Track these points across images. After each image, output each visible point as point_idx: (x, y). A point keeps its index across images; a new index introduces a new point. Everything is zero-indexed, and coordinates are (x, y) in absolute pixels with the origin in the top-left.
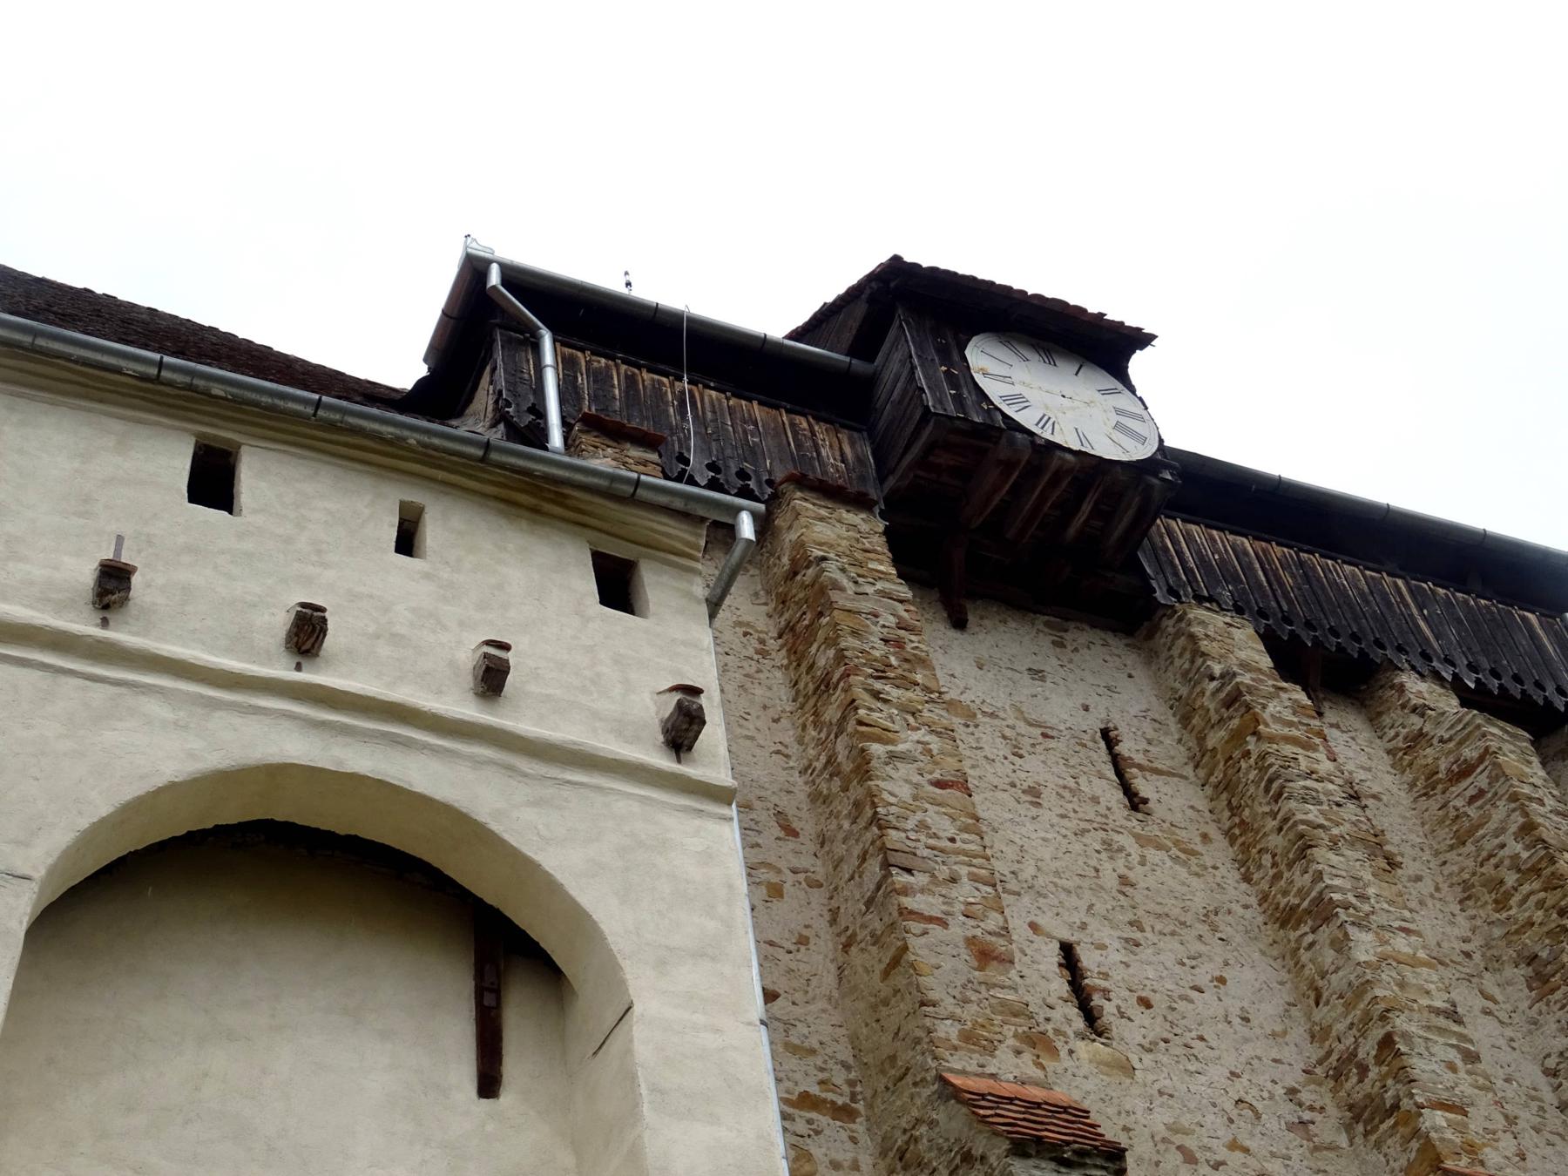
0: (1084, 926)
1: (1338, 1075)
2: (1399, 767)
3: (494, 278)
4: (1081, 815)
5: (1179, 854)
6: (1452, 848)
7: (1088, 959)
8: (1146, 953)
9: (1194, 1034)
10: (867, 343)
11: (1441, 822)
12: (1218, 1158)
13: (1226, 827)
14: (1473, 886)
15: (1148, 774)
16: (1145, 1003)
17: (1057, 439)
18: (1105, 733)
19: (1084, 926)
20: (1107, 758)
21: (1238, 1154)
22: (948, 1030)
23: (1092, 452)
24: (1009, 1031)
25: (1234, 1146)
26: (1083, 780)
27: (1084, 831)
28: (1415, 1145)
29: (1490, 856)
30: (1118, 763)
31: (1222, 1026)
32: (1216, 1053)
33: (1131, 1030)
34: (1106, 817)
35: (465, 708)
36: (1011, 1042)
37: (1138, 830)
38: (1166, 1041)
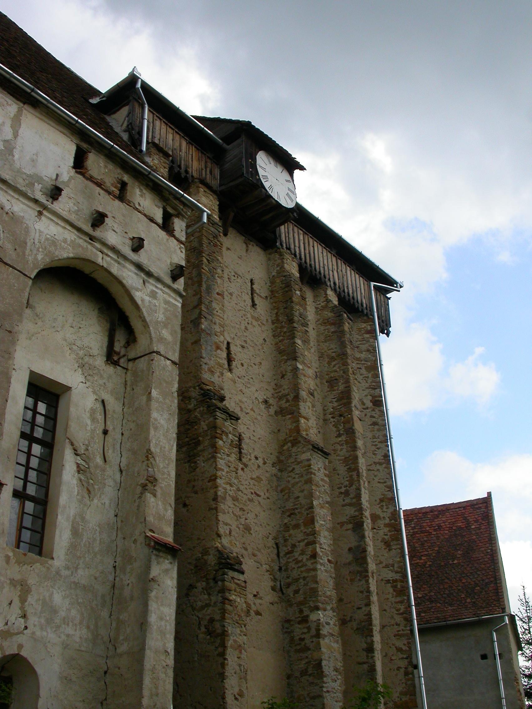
0: (233, 338)
1: (280, 398)
2: (316, 313)
3: (139, 85)
4: (240, 305)
5: (260, 324)
6: (323, 342)
7: (232, 348)
8: (246, 350)
9: (251, 377)
10: (229, 139)
11: (322, 334)
12: (248, 412)
13: (273, 319)
14: (324, 355)
15: (259, 297)
16: (242, 365)
17: (272, 194)
18: (252, 280)
19: (233, 338)
20: (250, 289)
21: (252, 412)
22: (205, 367)
23: (280, 202)
24: (218, 370)
25: (252, 409)
26: (243, 294)
27: (240, 310)
28: (294, 424)
29: (332, 349)
30: (252, 290)
31: (258, 376)
32: (254, 383)
33: (238, 371)
34: (246, 307)
35: (127, 250)
36: (218, 374)
37: (252, 313)
38: (244, 377)
